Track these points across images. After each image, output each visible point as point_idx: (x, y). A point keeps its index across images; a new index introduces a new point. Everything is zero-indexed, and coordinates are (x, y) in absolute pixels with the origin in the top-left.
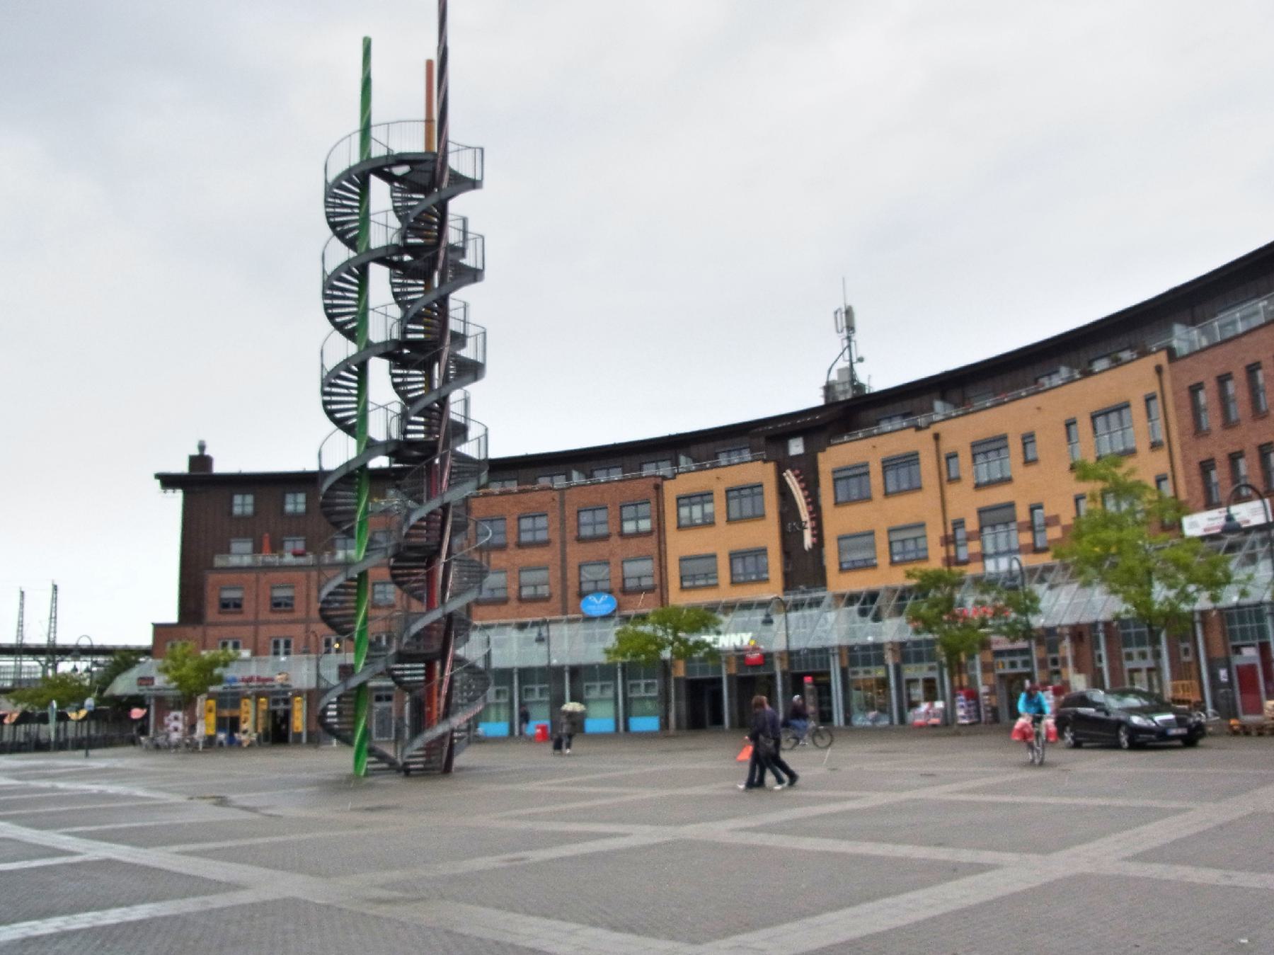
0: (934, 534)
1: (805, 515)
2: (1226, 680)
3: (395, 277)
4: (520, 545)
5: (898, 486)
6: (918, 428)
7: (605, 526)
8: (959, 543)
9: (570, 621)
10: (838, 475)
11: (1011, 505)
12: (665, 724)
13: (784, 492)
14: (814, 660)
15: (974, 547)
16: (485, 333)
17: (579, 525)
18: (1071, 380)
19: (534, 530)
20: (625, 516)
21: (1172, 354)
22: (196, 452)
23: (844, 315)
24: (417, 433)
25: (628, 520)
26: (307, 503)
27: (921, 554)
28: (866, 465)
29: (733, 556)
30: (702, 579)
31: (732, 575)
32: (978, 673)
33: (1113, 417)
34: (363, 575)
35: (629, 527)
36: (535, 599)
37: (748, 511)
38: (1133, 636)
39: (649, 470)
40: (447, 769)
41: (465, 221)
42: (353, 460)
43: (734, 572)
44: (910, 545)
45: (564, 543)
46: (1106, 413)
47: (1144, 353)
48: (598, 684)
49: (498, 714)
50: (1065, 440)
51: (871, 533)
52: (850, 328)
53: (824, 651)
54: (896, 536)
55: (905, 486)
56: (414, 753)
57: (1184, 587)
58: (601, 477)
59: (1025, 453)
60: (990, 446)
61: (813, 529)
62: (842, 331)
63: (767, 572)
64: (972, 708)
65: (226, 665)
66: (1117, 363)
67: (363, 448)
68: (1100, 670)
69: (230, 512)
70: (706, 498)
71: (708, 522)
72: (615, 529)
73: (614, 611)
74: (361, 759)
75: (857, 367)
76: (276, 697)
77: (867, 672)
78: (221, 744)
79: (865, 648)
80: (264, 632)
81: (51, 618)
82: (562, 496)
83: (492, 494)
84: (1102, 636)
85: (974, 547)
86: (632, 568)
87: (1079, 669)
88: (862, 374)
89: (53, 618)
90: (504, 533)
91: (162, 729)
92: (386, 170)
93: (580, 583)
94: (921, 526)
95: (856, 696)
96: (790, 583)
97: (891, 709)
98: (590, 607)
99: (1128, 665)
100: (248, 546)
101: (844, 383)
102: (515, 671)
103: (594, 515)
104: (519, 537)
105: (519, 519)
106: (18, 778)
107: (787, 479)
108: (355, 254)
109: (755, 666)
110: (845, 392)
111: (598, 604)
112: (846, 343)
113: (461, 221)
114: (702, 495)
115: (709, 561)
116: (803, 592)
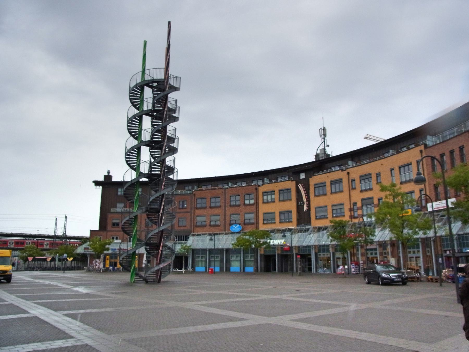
0: (347, 208)
1: (305, 200)
2: (441, 262)
3: (129, 124)
4: (211, 207)
5: (336, 190)
6: (343, 170)
7: (219, 203)
8: (355, 211)
9: (226, 234)
11: (372, 198)
12: (256, 270)
13: (298, 191)
14: (306, 250)
15: (360, 212)
16: (178, 138)
17: (211, 203)
18: (393, 155)
20: (246, 198)
21: (426, 146)
22: (107, 174)
23: (323, 130)
24: (157, 171)
27: (342, 214)
28: (325, 183)
29: (281, 213)
30: (266, 221)
31: (280, 220)
32: (360, 256)
33: (406, 168)
34: (136, 217)
35: (247, 202)
37: (286, 198)
38: (445, 245)
39: (255, 183)
40: (159, 281)
41: (176, 101)
42: (134, 179)
43: (281, 219)
44: (339, 211)
45: (225, 207)
46: (404, 166)
47: (416, 146)
48: (235, 255)
49: (202, 264)
50: (390, 175)
51: (326, 207)
52: (325, 135)
53: (309, 247)
54: (334, 208)
55: (338, 190)
56: (148, 276)
57: (415, 229)
58: (239, 184)
59: (377, 180)
60: (366, 177)
61: (307, 204)
62: (322, 136)
63: (292, 219)
64: (357, 268)
65: (109, 244)
66: (409, 149)
67: (138, 175)
68: (400, 257)
69: (117, 194)
70: (273, 193)
71: (273, 201)
72: (242, 203)
73: (241, 231)
74: (133, 276)
75: (327, 148)
77: (324, 255)
78: (110, 270)
79: (324, 246)
81: (64, 227)
82: (225, 191)
83: (202, 190)
84: (400, 245)
85: (360, 212)
86: (247, 216)
87: (393, 257)
88: (329, 151)
89: (65, 227)
90: (206, 203)
91: (92, 265)
92: (151, 84)
93: (230, 221)
94: (343, 204)
95: (321, 263)
96: (299, 222)
97: (331, 268)
98: (233, 229)
99: (409, 255)
100: (122, 205)
101: (322, 154)
102: (208, 250)
103: (202, 201)
104: (211, 204)
106: (33, 278)
107: (299, 187)
108: (139, 112)
109: (287, 251)
110: (322, 157)
111: (236, 228)
112: (323, 140)
113: (175, 101)
114: (271, 192)
115: (273, 215)
116: (303, 226)
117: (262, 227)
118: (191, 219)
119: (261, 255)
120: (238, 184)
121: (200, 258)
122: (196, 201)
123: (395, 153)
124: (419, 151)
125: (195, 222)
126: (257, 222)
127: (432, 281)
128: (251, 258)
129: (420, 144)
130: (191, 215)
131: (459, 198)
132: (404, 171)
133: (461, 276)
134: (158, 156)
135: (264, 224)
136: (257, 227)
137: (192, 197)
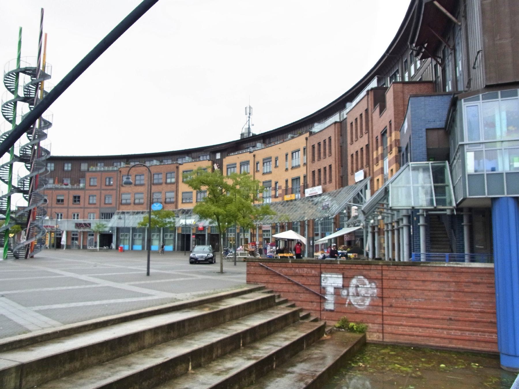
10: (228, 167)
11: (270, 181)
12: (174, 249)
19: (140, 180)
21: (311, 134)
25: (169, 178)
26: (54, 167)
33: (297, 153)
35: (169, 181)
36: (139, 204)
60: (267, 160)
76: (74, 233)
80: (71, 211)
86: (169, 195)
105: (136, 176)
109: (201, 231)
117: (181, 206)
118: (117, 196)
119: (178, 234)
120: (164, 161)
121: (138, 236)
122: (121, 178)
125: (120, 199)
126: (177, 201)
128: (170, 237)
130: (117, 193)
134: (482, 74)
135: (182, 203)
136: (176, 207)
137: (118, 174)
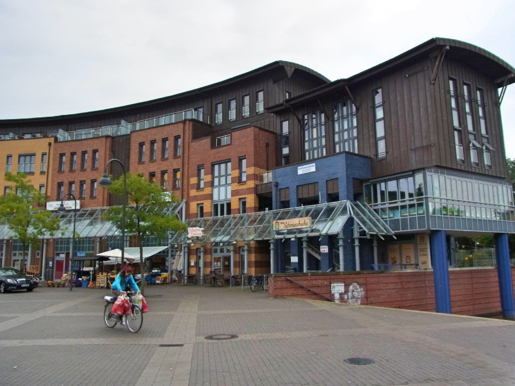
2: (51, 266)
18: (13, 139)
21: (56, 139)
33: (28, 158)
46: (25, 156)
47: (46, 136)
66: (34, 137)
99: (14, 258)
123: (17, 138)
124: (47, 144)
127: (54, 286)
129: (50, 136)
131: (83, 201)
132: (25, 161)
133: (85, 280)
